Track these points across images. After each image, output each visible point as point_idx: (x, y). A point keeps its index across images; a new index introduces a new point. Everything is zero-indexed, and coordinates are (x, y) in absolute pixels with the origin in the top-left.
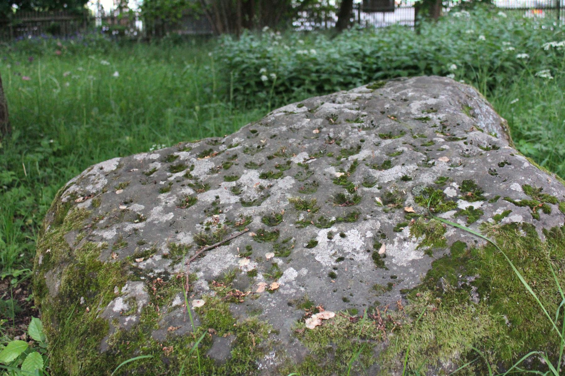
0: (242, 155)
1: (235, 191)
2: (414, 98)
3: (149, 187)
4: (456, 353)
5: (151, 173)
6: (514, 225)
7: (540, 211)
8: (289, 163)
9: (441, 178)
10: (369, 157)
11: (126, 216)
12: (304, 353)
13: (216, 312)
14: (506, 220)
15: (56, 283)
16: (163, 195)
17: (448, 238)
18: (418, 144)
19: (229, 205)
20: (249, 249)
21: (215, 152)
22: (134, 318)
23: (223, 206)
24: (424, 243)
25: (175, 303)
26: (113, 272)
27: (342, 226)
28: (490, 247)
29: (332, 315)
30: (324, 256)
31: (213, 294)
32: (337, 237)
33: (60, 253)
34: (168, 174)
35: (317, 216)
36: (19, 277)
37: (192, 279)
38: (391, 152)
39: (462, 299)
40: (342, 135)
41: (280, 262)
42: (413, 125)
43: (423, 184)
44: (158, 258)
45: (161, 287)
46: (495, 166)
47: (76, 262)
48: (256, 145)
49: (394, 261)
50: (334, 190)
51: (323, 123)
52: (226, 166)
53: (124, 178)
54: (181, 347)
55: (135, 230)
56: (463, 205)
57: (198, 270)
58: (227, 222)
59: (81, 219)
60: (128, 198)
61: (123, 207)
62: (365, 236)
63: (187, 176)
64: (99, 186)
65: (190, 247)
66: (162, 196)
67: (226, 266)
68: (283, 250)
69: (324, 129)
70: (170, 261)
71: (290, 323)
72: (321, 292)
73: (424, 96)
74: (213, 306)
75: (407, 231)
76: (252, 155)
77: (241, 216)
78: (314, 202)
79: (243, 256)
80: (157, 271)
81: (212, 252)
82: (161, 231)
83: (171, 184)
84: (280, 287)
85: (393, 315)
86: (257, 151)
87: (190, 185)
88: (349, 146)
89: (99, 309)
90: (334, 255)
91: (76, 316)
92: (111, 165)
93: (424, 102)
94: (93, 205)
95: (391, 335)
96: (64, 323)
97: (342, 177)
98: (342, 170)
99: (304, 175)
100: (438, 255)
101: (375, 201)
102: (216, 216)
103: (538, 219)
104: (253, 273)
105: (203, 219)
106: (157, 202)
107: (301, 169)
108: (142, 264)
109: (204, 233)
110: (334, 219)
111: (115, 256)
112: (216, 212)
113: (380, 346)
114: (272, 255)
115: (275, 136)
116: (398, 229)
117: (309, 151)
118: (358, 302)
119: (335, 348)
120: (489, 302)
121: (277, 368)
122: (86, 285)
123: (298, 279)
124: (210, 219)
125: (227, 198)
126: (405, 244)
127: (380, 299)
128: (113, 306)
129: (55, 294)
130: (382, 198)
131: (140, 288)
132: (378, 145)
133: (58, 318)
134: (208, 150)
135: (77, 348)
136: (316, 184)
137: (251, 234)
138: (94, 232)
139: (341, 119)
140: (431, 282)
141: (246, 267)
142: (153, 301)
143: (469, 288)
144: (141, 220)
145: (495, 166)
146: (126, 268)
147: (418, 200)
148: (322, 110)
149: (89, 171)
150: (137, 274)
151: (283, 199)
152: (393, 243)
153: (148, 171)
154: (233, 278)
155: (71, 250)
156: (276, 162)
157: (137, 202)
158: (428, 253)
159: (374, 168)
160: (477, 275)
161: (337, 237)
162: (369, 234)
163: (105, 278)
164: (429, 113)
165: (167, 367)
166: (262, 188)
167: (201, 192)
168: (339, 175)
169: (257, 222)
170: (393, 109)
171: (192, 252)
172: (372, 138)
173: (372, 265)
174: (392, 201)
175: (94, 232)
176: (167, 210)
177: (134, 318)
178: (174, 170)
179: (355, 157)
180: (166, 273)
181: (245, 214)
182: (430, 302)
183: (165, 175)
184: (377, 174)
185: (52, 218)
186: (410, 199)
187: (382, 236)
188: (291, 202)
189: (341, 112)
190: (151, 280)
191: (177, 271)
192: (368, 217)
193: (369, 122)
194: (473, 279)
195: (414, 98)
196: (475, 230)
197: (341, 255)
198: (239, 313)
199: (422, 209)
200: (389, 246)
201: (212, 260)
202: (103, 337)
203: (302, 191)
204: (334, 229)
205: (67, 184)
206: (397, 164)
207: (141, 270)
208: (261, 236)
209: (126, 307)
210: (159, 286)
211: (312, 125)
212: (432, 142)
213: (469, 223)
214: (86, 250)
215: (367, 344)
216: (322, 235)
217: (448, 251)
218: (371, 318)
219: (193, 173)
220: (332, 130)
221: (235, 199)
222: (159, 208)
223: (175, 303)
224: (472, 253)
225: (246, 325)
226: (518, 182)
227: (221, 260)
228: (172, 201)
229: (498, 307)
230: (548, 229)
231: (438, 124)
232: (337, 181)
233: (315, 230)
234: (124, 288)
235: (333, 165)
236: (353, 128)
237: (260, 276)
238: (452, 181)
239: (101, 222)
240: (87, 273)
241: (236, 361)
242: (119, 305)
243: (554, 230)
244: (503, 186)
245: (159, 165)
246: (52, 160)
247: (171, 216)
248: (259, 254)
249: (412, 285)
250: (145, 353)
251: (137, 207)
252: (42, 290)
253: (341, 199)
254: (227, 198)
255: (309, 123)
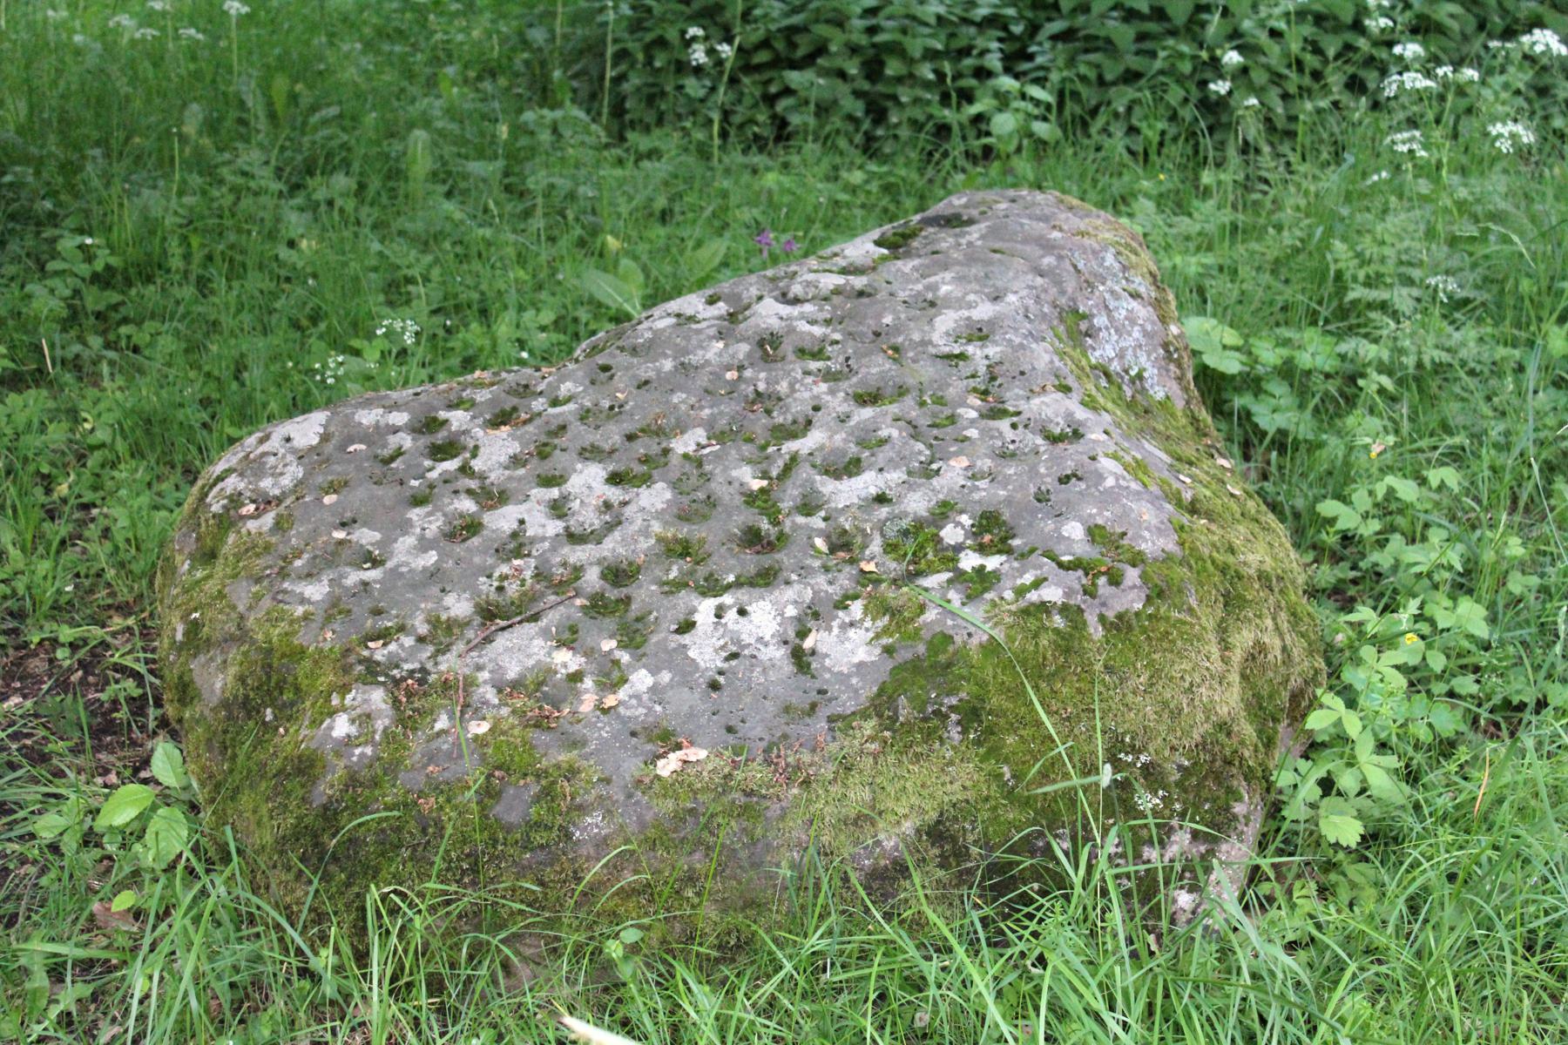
0: (576, 427)
1: (558, 509)
2: (949, 303)
3: (388, 493)
4: (908, 827)
5: (392, 459)
6: (1044, 607)
7: (1102, 580)
8: (666, 452)
9: (944, 504)
10: (821, 448)
11: (346, 553)
12: (649, 817)
13: (509, 744)
14: (1033, 596)
15: (217, 680)
16: (417, 510)
17: (926, 624)
18: (924, 422)
19: (544, 539)
20: (573, 630)
21: (524, 416)
22: (369, 750)
23: (533, 541)
24: (886, 631)
25: (438, 726)
26: (327, 667)
27: (743, 595)
28: (991, 648)
29: (702, 754)
30: (704, 650)
31: (505, 711)
32: (731, 615)
33: (218, 624)
34: (427, 463)
35: (702, 571)
36: (74, 647)
37: (470, 683)
38: (870, 441)
39: (929, 736)
40: (783, 387)
41: (625, 657)
42: (927, 371)
43: (906, 514)
44: (408, 641)
45: (414, 695)
46: (1050, 482)
47: (253, 642)
48: (606, 404)
49: (827, 662)
50: (742, 517)
51: (749, 355)
52: (543, 453)
53: (338, 468)
54: (448, 801)
55: (365, 584)
56: (969, 561)
57: (479, 668)
58: (539, 575)
59: (258, 555)
60: (348, 514)
61: (340, 535)
62: (782, 614)
63: (465, 470)
64: (286, 481)
65: (468, 624)
66: (415, 514)
67: (531, 662)
68: (633, 637)
69: (748, 373)
70: (431, 649)
71: (632, 767)
72: (691, 715)
73: (972, 297)
74: (504, 733)
75: (857, 608)
76: (597, 427)
77: (564, 565)
78: (702, 542)
79: (562, 644)
80: (407, 667)
81: (506, 634)
82: (414, 587)
83: (431, 486)
84: (620, 703)
85: (806, 757)
86: (609, 418)
87: (469, 492)
88: (790, 418)
89: (303, 732)
90: (723, 648)
91: (259, 743)
92: (307, 430)
93: (966, 313)
94: (278, 526)
95: (795, 791)
96: (235, 756)
97: (762, 490)
98: (765, 475)
99: (694, 480)
100: (904, 655)
101: (813, 546)
102: (516, 562)
103: (1093, 596)
104: (576, 677)
105: (493, 567)
106: (405, 527)
107: (688, 467)
108: (380, 652)
109: (493, 596)
110: (731, 578)
111: (329, 635)
112: (517, 553)
113: (775, 809)
114: (613, 644)
115: (646, 382)
116: (841, 605)
117: (709, 425)
118: (752, 734)
119: (702, 810)
120: (978, 743)
121: (605, 838)
122: (274, 687)
123: (653, 690)
124: (504, 569)
125: (543, 526)
126: (852, 633)
127: (791, 729)
128: (331, 728)
129: (215, 701)
130: (828, 538)
131: (377, 697)
132: (843, 419)
133: (223, 745)
134: (508, 408)
135: (268, 799)
136: (711, 502)
137: (578, 602)
138: (286, 585)
139: (787, 348)
140: (882, 705)
141: (565, 666)
142: (401, 721)
143: (947, 717)
144: (376, 563)
145: (1050, 482)
146: (352, 659)
147: (890, 548)
148: (752, 321)
149: (261, 441)
150: (373, 671)
151: (645, 532)
152: (829, 629)
153: (386, 453)
154: (541, 684)
155: (242, 617)
156: (640, 448)
157: (365, 524)
158: (888, 650)
159: (827, 472)
160: (963, 695)
161: (731, 615)
162: (791, 611)
163: (311, 675)
164: (970, 341)
165: (424, 831)
166: (608, 505)
167: (492, 508)
168: (757, 484)
169: (592, 578)
170: (897, 329)
171: (470, 634)
172: (837, 403)
173: (788, 668)
174: (846, 546)
175: (286, 585)
176: (424, 545)
177: (369, 750)
178: (441, 452)
179: (790, 446)
180: (423, 670)
181: (572, 560)
182: (872, 739)
183: (420, 465)
184: (827, 486)
185: (191, 545)
186: (876, 546)
187: (813, 615)
188: (660, 540)
189: (792, 330)
190: (396, 682)
191: (443, 667)
192: (794, 577)
193: (841, 359)
194: (954, 701)
195: (949, 303)
196: (975, 614)
197: (734, 649)
198: (548, 746)
199: (894, 565)
200: (823, 634)
201: (507, 650)
202: (314, 780)
203: (684, 517)
204: (727, 599)
205: (219, 468)
206: (870, 467)
207: (378, 663)
208: (598, 606)
209: (353, 730)
210: (410, 694)
211: (726, 359)
212: (952, 419)
213: (970, 598)
214: (273, 621)
215: (750, 806)
216: (705, 609)
217: (921, 649)
218: (768, 762)
219: (477, 465)
220: (763, 375)
221: (555, 527)
222: (409, 541)
223: (438, 726)
224: (962, 654)
225: (558, 767)
226: (1081, 520)
227: (523, 650)
228: (435, 526)
229: (993, 752)
230: (1111, 615)
231: (982, 370)
232: (751, 498)
233: (694, 600)
234: (349, 697)
235: (749, 462)
236: (807, 373)
237: (588, 683)
238: (962, 512)
239: (298, 563)
240: (276, 663)
241: (538, 825)
242: (342, 727)
243: (1120, 616)
244: (1050, 525)
245: (406, 441)
246: (94, 300)
247: (432, 558)
248: (589, 642)
249: (851, 706)
250: (387, 808)
251: (366, 537)
252: (186, 691)
253: (752, 538)
254: (543, 526)
255: (720, 355)
